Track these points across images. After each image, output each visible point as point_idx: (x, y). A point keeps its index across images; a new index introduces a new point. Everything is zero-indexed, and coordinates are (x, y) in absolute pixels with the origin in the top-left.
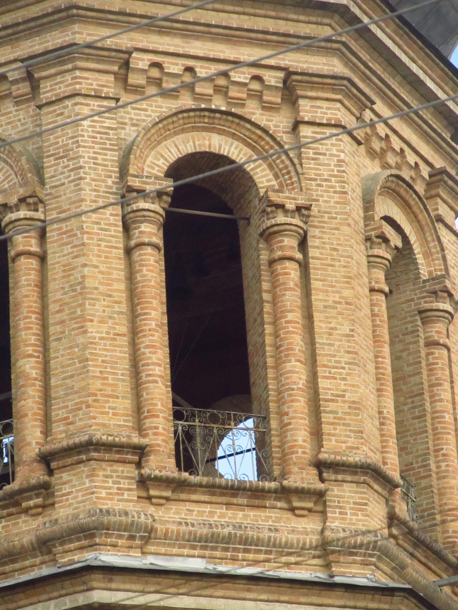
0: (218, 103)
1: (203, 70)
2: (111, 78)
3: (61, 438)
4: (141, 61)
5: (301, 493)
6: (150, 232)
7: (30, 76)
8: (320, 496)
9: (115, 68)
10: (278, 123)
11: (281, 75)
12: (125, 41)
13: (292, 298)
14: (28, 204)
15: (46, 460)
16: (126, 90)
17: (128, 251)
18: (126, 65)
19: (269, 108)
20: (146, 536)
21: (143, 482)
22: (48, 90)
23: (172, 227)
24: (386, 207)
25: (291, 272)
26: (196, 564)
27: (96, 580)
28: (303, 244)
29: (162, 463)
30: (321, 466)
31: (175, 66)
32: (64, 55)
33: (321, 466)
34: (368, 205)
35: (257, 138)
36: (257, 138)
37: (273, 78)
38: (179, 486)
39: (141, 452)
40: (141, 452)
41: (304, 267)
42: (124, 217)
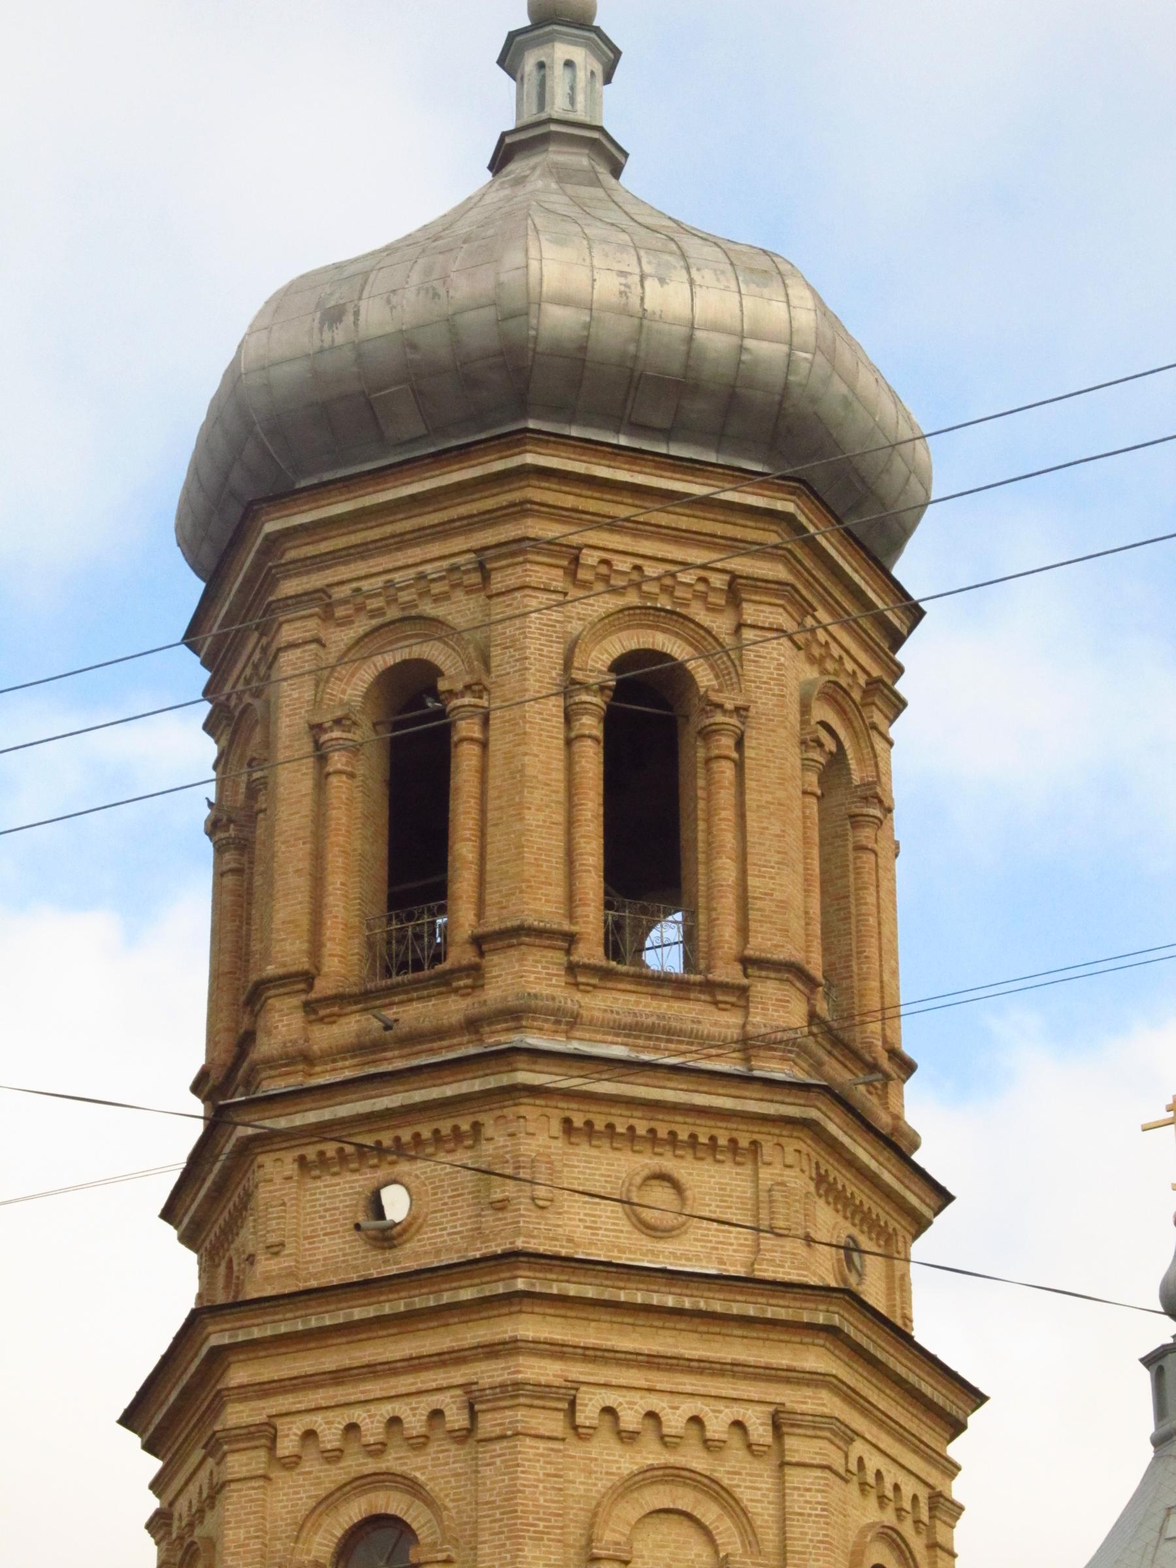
0: (664, 602)
1: (651, 570)
2: (560, 572)
3: (494, 922)
4: (590, 558)
5: (725, 987)
6: (591, 724)
7: (481, 567)
8: (743, 991)
9: (565, 563)
10: (721, 624)
11: (727, 577)
12: (316, 580)
13: (726, 796)
14: (473, 692)
15: (479, 942)
16: (574, 584)
17: (569, 742)
18: (576, 560)
19: (712, 609)
20: (571, 1021)
21: (572, 969)
22: (499, 581)
23: (612, 720)
24: (822, 712)
25: (726, 771)
26: (619, 1051)
27: (521, 1061)
28: (739, 745)
29: (591, 951)
30: (746, 962)
31: (623, 564)
32: (517, 548)
33: (746, 962)
34: (805, 708)
35: (701, 637)
36: (701, 637)
37: (718, 581)
38: (606, 974)
39: (571, 939)
40: (571, 939)
41: (740, 766)
42: (566, 708)
